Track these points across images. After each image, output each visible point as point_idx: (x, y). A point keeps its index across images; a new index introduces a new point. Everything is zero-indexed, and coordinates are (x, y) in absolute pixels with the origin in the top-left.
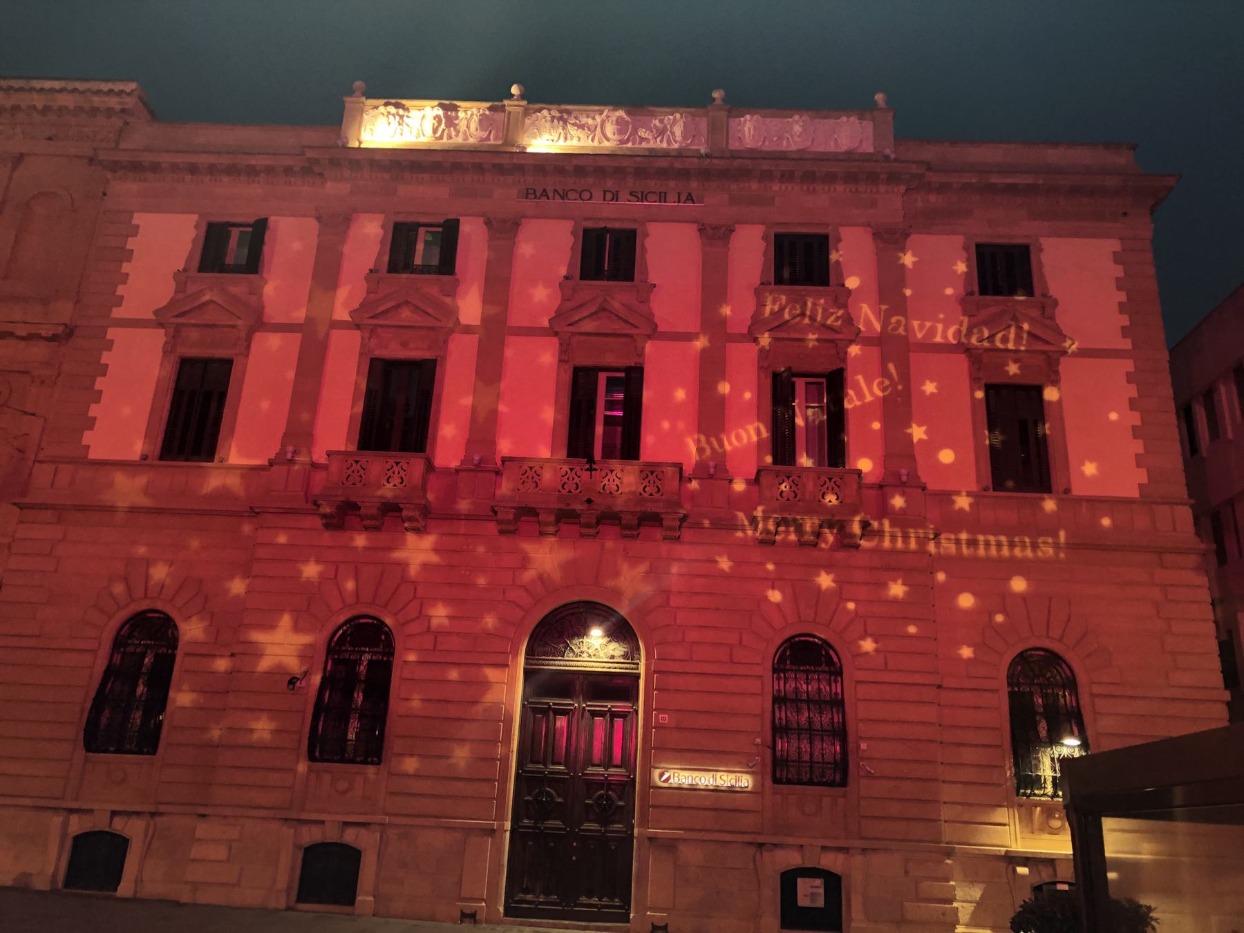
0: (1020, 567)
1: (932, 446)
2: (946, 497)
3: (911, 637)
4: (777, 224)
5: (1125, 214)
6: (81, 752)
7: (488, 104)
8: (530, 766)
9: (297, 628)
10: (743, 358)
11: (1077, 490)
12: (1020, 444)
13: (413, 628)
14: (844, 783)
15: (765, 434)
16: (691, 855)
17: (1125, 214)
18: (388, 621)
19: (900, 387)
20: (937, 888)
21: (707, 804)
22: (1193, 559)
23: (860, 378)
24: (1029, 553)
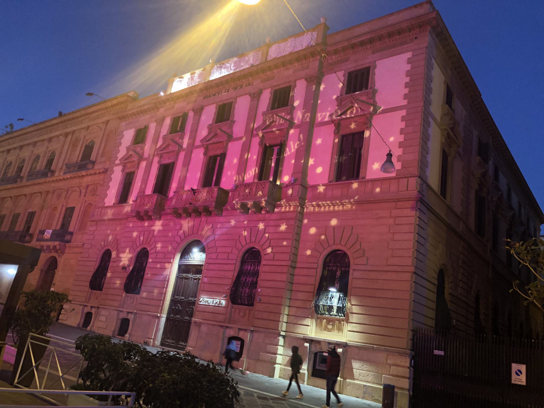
0: (334, 214)
1: (315, 166)
2: (315, 187)
3: (284, 246)
4: (275, 86)
5: (416, 38)
6: (87, 289)
7: (190, 73)
8: (176, 297)
9: (130, 253)
10: (256, 143)
11: (369, 177)
12: (350, 158)
13: (153, 251)
14: (252, 305)
15: (257, 171)
16: (204, 328)
17: (416, 38)
18: (148, 249)
19: (303, 144)
20: (270, 348)
21: (211, 311)
22: (411, 203)
23: (292, 143)
24: (341, 208)
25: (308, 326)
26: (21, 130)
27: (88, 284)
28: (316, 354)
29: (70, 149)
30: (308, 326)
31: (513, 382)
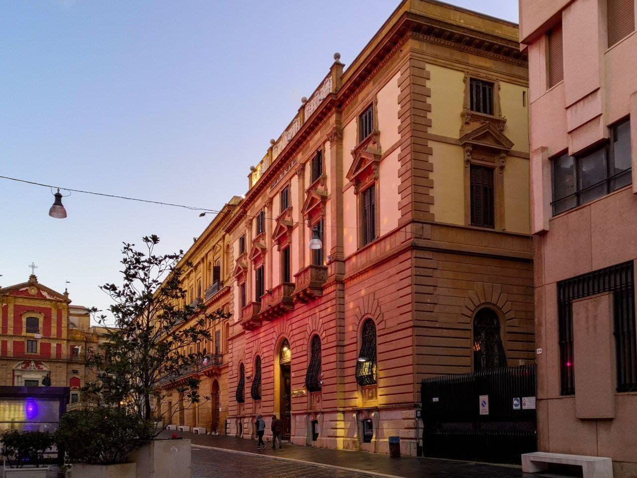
25: (357, 398)
26: (356, 61)
27: (235, 398)
28: (363, 422)
29: (208, 272)
30: (357, 398)
31: (481, 414)
